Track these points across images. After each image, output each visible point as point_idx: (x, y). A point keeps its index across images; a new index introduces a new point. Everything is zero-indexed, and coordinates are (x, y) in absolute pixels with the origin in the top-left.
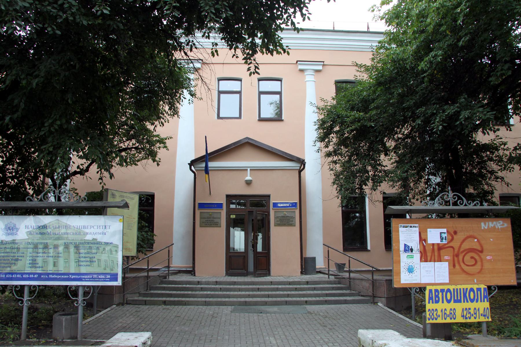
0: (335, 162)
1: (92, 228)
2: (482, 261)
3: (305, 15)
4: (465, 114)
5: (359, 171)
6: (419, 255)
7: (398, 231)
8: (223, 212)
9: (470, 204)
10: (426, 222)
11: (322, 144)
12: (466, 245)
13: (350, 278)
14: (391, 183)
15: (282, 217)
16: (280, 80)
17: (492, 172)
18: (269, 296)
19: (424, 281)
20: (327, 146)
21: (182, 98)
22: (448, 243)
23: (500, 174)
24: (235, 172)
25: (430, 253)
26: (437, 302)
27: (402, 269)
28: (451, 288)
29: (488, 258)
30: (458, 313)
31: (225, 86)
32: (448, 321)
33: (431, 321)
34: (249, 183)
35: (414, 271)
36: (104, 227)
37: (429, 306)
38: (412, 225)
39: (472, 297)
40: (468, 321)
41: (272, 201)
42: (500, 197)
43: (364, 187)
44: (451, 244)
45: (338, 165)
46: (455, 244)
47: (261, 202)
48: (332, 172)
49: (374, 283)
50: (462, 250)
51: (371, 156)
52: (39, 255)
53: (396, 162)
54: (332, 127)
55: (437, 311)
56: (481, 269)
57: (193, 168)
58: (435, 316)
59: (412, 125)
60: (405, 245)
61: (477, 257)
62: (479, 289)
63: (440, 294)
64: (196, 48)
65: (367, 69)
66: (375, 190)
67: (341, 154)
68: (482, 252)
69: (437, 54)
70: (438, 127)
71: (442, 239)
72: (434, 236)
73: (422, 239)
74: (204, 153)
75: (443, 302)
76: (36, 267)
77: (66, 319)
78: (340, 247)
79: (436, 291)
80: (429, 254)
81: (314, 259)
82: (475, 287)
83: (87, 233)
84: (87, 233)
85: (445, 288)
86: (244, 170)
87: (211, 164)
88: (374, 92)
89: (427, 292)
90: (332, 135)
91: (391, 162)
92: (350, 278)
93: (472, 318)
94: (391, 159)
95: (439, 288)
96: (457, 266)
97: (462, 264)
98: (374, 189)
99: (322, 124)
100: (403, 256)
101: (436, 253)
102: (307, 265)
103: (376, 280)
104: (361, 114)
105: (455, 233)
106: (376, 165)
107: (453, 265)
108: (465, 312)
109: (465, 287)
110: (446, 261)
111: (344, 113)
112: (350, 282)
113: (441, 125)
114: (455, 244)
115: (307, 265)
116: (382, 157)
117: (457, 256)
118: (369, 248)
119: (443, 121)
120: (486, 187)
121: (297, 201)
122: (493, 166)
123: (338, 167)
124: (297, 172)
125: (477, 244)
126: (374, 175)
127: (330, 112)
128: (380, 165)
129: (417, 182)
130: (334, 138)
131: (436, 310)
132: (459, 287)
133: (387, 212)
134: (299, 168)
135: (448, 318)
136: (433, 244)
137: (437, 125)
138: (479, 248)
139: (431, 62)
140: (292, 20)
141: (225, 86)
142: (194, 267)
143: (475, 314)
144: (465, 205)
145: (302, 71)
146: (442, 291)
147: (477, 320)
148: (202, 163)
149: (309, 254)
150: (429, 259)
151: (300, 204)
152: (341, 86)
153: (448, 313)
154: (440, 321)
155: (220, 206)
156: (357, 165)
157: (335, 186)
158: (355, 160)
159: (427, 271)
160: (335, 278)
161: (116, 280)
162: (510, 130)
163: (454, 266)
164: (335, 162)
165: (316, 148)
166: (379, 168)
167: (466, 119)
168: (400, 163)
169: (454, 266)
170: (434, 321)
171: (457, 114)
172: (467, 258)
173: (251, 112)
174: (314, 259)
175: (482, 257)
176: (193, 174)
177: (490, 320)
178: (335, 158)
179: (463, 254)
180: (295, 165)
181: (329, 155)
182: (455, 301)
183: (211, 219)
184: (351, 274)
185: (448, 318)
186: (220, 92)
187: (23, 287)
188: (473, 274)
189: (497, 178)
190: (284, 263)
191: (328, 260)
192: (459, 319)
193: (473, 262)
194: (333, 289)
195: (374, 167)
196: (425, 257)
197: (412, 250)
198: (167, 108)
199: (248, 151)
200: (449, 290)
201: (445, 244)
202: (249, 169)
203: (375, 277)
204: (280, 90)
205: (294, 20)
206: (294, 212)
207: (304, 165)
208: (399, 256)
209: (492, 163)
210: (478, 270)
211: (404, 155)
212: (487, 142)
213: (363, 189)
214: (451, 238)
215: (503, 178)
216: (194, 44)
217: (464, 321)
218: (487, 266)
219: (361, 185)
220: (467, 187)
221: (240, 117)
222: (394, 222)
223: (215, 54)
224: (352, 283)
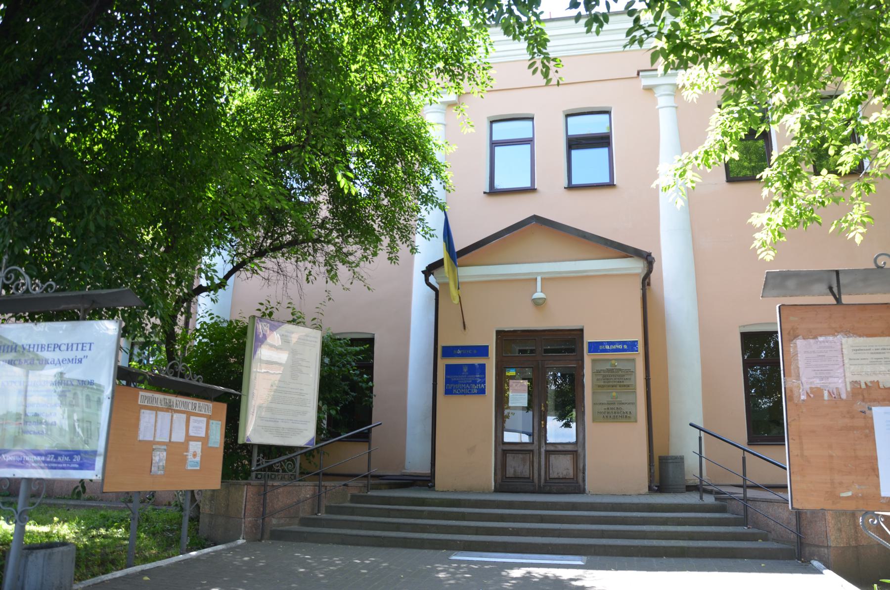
1: (57, 349)
13: (745, 499)
16: (607, 112)
31: (503, 131)
34: (538, 304)
36: (80, 346)
41: (588, 338)
47: (568, 342)
57: (432, 279)
78: (741, 435)
121: (639, 337)
141: (503, 131)
145: (649, 89)
155: (482, 351)
160: (716, 499)
176: (434, 292)
180: (636, 266)
183: (616, 406)
184: (748, 490)
186: (494, 144)
194: (709, 522)
199: (539, 241)
202: (539, 279)
206: (634, 360)
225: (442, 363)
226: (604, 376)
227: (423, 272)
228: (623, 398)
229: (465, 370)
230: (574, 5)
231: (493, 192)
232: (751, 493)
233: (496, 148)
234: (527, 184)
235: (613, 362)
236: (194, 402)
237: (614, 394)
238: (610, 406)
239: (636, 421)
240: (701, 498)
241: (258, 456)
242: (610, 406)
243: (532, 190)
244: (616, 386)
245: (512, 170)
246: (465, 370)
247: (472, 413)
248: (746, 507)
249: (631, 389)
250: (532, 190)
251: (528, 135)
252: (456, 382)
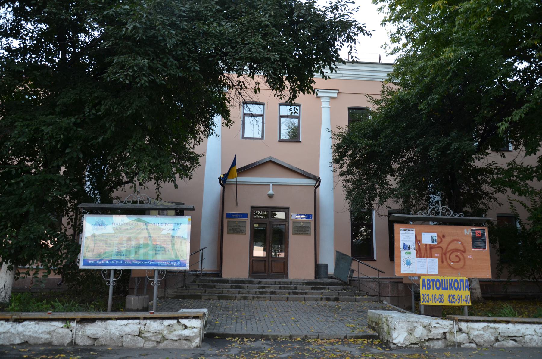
0: (348, 181)
2: (464, 259)
3: (333, 68)
4: (455, 145)
5: (367, 189)
6: (415, 252)
7: (399, 233)
8: (248, 221)
9: (456, 215)
10: (421, 227)
11: (337, 166)
12: (452, 247)
14: (395, 199)
15: (300, 227)
17: (487, 194)
19: (419, 272)
20: (341, 167)
21: (229, 125)
22: (438, 244)
23: (495, 195)
24: (259, 186)
25: (423, 251)
26: (429, 289)
27: (402, 262)
28: (440, 278)
29: (470, 257)
30: (446, 298)
32: (438, 304)
33: (424, 303)
34: (271, 196)
35: (411, 264)
37: (423, 292)
38: (410, 229)
39: (456, 286)
40: (453, 304)
42: (497, 217)
43: (372, 202)
44: (441, 245)
45: (350, 183)
46: (444, 245)
48: (345, 189)
50: (449, 249)
51: (379, 176)
52: (123, 245)
53: (400, 181)
54: (346, 151)
55: (429, 296)
56: (464, 265)
58: (428, 300)
59: (413, 149)
60: (404, 244)
61: (461, 256)
62: (462, 281)
63: (431, 282)
64: (246, 87)
65: (378, 102)
66: (382, 205)
67: (353, 174)
68: (464, 252)
69: (435, 97)
70: (434, 154)
71: (433, 241)
72: (427, 238)
73: (418, 240)
75: (433, 289)
76: (120, 255)
77: (134, 299)
79: (428, 280)
80: (423, 252)
81: (326, 266)
82: (459, 279)
83: (163, 229)
84: (163, 229)
85: (436, 278)
88: (383, 123)
89: (421, 281)
90: (346, 158)
91: (396, 182)
93: (456, 302)
94: (396, 179)
95: (430, 278)
96: (445, 262)
97: (449, 260)
98: (381, 203)
99: (337, 148)
100: (403, 253)
101: (428, 252)
104: (372, 141)
105: (444, 236)
106: (383, 183)
107: (441, 261)
108: (451, 298)
109: (451, 278)
110: (436, 257)
111: (358, 140)
113: (436, 153)
114: (444, 245)
116: (389, 177)
117: (445, 254)
118: (375, 258)
119: (438, 150)
120: (481, 206)
121: (313, 214)
122: (486, 188)
123: (350, 185)
125: (461, 246)
126: (382, 192)
127: (344, 138)
128: (386, 184)
129: (418, 200)
130: (347, 160)
131: (428, 295)
132: (446, 278)
133: (391, 219)
135: (438, 302)
136: (426, 245)
137: (433, 154)
138: (462, 249)
139: (428, 104)
140: (321, 70)
142: (221, 270)
143: (459, 299)
144: (452, 216)
146: (433, 280)
147: (460, 304)
149: (321, 261)
150: (423, 255)
151: (315, 216)
152: (355, 114)
153: (437, 297)
154: (431, 303)
155: (245, 216)
156: (367, 183)
157: (348, 201)
158: (365, 179)
159: (421, 265)
161: (185, 265)
162: (504, 157)
163: (442, 262)
164: (348, 181)
165: (332, 168)
166: (386, 186)
167: (455, 150)
168: (402, 183)
169: (442, 262)
170: (427, 304)
171: (449, 144)
172: (453, 256)
173: (276, 136)
174: (326, 266)
175: (465, 256)
177: (470, 304)
178: (348, 177)
179: (450, 253)
181: (342, 174)
182: (443, 289)
185: (438, 302)
187: (110, 270)
188: (456, 269)
189: (491, 198)
190: (300, 269)
192: (446, 303)
193: (457, 260)
195: (381, 186)
196: (419, 254)
197: (409, 248)
198: (202, 128)
199: (270, 168)
200: (438, 280)
201: (435, 245)
202: (271, 184)
205: (323, 70)
206: (310, 223)
208: (400, 252)
209: (487, 185)
210: (461, 266)
211: (406, 176)
212: (484, 166)
213: (371, 204)
214: (440, 240)
215: (496, 198)
216: (244, 84)
217: (450, 304)
218: (468, 263)
219: (370, 201)
220: (465, 206)
221: (262, 138)
222: (396, 226)
223: (258, 91)
233: (284, 218)
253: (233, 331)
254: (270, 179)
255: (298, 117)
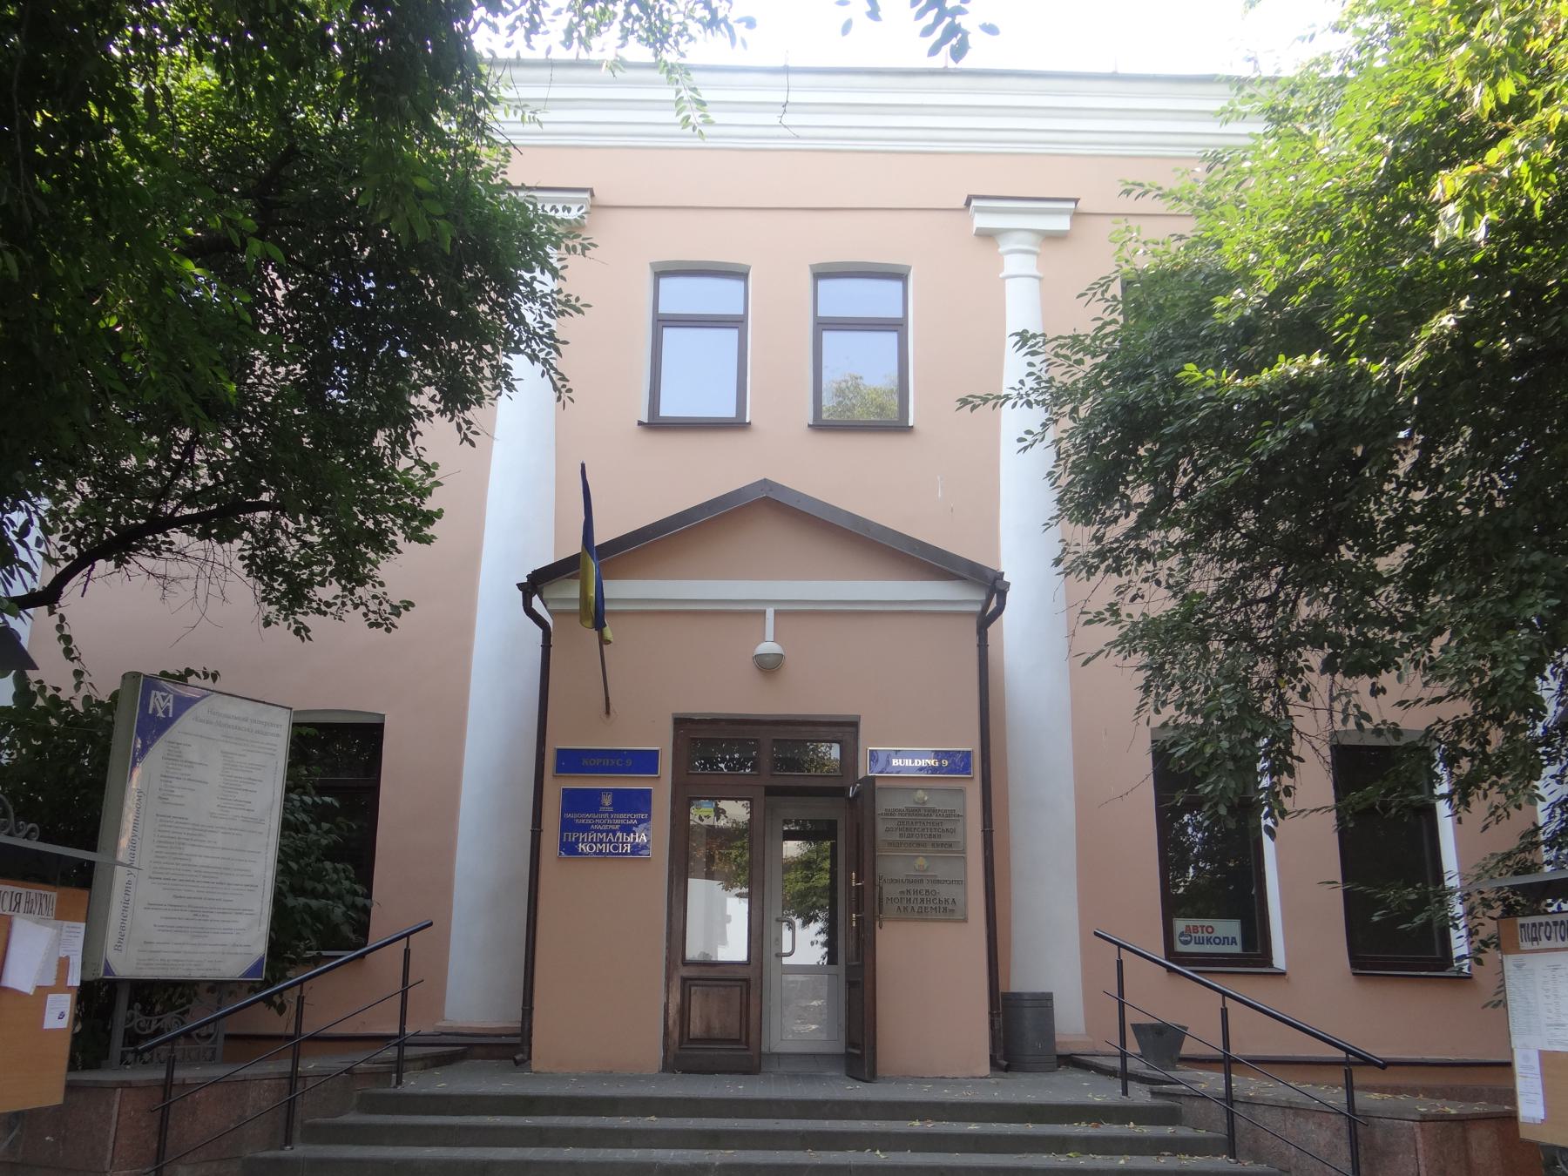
18: (714, 1140)
31: (681, 296)
34: (769, 667)
49: (1355, 1122)
57: (537, 603)
74: (575, 547)
86: (750, 614)
87: (616, 590)
92: (1229, 1098)
102: (1017, 1029)
103: (1367, 1116)
112: (1231, 1116)
115: (1017, 1029)
118: (1279, 960)
121: (972, 745)
124: (972, 625)
134: (978, 608)
141: (681, 296)
145: (988, 236)
148: (575, 586)
149: (1021, 981)
151: (983, 762)
155: (645, 762)
160: (1154, 1094)
186: (662, 322)
191: (1122, 1005)
199: (772, 537)
202: (770, 612)
203: (1364, 1099)
204: (898, 314)
206: (961, 791)
207: (1002, 595)
224: (1240, 1123)
225: (554, 789)
226: (901, 822)
227: (520, 586)
228: (942, 870)
229: (607, 801)
230: (1453, 3)
231: (656, 424)
232: (1248, 1085)
233: (665, 331)
234: (730, 412)
235: (920, 794)
236: (17, 890)
237: (921, 862)
238: (911, 887)
239: (965, 920)
240: (1125, 1092)
241: (130, 1007)
242: (911, 887)
243: (737, 425)
244: (924, 845)
245: (698, 378)
246: (607, 801)
247: (606, 897)
248: (1231, 1116)
249: (953, 850)
250: (737, 425)
251: (895, 312)
252: (585, 828)
253: (1186, 220)
254: (769, 583)
255: (897, 326)
